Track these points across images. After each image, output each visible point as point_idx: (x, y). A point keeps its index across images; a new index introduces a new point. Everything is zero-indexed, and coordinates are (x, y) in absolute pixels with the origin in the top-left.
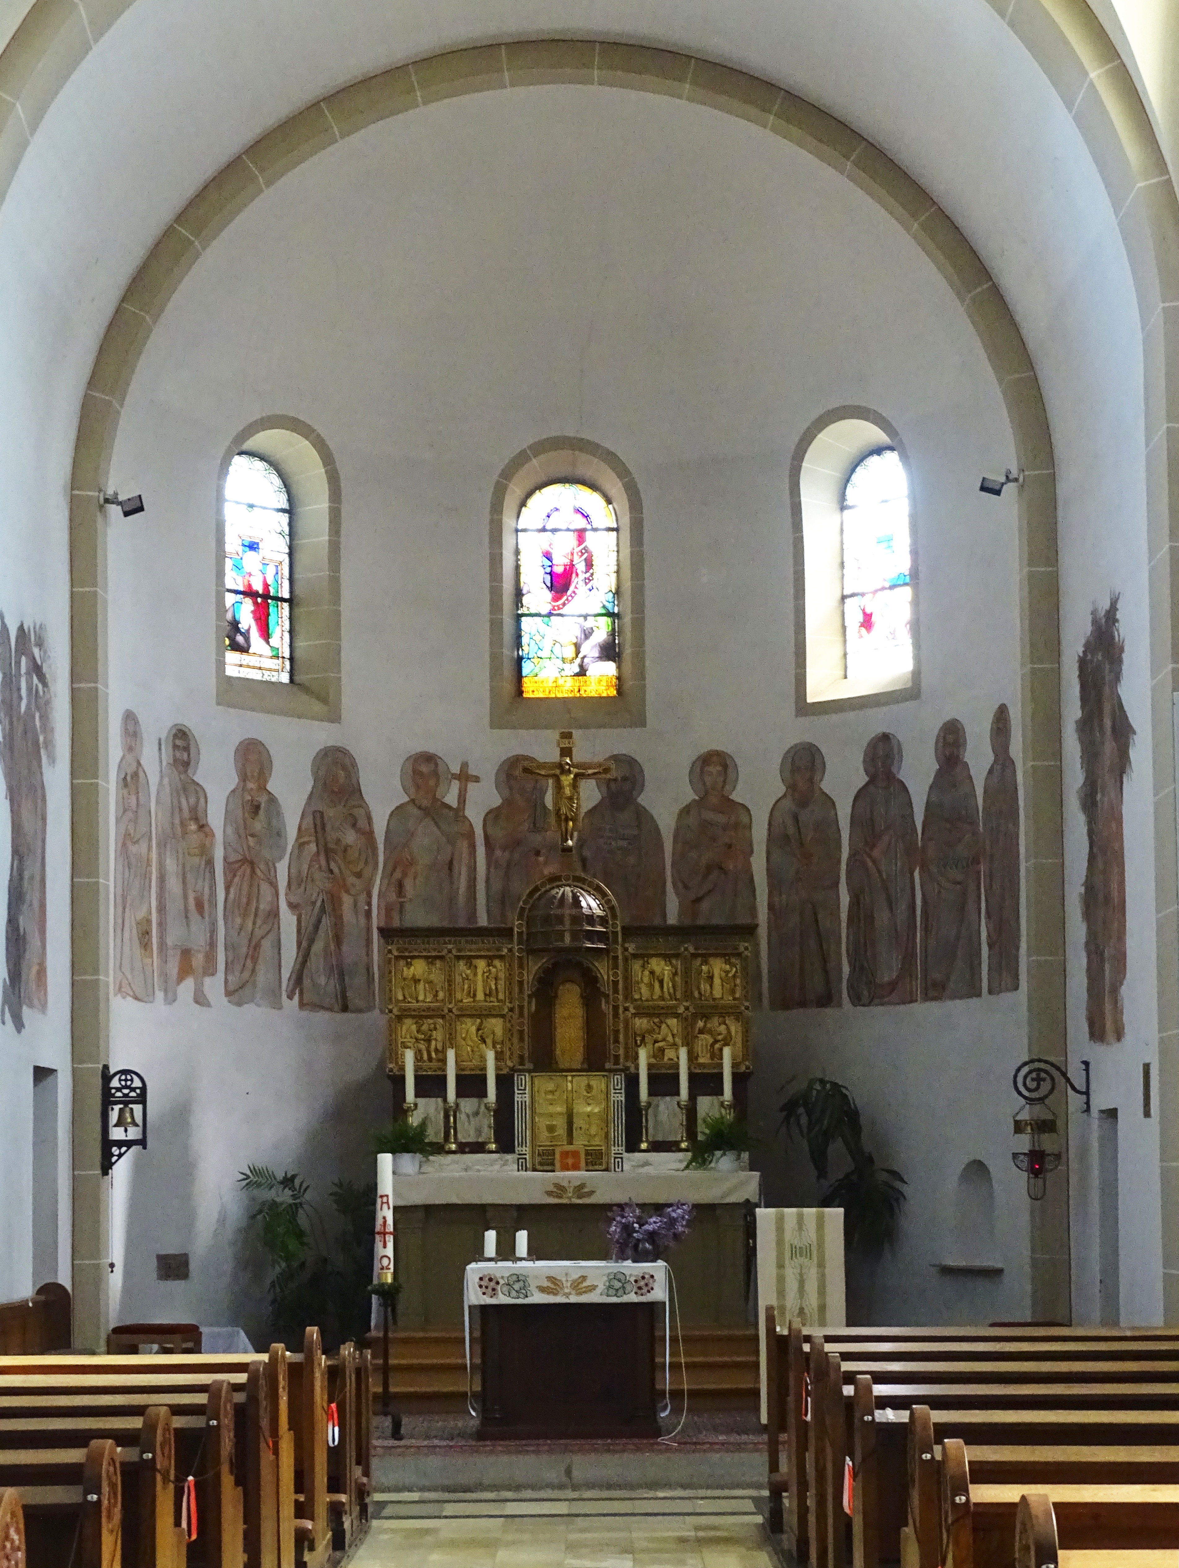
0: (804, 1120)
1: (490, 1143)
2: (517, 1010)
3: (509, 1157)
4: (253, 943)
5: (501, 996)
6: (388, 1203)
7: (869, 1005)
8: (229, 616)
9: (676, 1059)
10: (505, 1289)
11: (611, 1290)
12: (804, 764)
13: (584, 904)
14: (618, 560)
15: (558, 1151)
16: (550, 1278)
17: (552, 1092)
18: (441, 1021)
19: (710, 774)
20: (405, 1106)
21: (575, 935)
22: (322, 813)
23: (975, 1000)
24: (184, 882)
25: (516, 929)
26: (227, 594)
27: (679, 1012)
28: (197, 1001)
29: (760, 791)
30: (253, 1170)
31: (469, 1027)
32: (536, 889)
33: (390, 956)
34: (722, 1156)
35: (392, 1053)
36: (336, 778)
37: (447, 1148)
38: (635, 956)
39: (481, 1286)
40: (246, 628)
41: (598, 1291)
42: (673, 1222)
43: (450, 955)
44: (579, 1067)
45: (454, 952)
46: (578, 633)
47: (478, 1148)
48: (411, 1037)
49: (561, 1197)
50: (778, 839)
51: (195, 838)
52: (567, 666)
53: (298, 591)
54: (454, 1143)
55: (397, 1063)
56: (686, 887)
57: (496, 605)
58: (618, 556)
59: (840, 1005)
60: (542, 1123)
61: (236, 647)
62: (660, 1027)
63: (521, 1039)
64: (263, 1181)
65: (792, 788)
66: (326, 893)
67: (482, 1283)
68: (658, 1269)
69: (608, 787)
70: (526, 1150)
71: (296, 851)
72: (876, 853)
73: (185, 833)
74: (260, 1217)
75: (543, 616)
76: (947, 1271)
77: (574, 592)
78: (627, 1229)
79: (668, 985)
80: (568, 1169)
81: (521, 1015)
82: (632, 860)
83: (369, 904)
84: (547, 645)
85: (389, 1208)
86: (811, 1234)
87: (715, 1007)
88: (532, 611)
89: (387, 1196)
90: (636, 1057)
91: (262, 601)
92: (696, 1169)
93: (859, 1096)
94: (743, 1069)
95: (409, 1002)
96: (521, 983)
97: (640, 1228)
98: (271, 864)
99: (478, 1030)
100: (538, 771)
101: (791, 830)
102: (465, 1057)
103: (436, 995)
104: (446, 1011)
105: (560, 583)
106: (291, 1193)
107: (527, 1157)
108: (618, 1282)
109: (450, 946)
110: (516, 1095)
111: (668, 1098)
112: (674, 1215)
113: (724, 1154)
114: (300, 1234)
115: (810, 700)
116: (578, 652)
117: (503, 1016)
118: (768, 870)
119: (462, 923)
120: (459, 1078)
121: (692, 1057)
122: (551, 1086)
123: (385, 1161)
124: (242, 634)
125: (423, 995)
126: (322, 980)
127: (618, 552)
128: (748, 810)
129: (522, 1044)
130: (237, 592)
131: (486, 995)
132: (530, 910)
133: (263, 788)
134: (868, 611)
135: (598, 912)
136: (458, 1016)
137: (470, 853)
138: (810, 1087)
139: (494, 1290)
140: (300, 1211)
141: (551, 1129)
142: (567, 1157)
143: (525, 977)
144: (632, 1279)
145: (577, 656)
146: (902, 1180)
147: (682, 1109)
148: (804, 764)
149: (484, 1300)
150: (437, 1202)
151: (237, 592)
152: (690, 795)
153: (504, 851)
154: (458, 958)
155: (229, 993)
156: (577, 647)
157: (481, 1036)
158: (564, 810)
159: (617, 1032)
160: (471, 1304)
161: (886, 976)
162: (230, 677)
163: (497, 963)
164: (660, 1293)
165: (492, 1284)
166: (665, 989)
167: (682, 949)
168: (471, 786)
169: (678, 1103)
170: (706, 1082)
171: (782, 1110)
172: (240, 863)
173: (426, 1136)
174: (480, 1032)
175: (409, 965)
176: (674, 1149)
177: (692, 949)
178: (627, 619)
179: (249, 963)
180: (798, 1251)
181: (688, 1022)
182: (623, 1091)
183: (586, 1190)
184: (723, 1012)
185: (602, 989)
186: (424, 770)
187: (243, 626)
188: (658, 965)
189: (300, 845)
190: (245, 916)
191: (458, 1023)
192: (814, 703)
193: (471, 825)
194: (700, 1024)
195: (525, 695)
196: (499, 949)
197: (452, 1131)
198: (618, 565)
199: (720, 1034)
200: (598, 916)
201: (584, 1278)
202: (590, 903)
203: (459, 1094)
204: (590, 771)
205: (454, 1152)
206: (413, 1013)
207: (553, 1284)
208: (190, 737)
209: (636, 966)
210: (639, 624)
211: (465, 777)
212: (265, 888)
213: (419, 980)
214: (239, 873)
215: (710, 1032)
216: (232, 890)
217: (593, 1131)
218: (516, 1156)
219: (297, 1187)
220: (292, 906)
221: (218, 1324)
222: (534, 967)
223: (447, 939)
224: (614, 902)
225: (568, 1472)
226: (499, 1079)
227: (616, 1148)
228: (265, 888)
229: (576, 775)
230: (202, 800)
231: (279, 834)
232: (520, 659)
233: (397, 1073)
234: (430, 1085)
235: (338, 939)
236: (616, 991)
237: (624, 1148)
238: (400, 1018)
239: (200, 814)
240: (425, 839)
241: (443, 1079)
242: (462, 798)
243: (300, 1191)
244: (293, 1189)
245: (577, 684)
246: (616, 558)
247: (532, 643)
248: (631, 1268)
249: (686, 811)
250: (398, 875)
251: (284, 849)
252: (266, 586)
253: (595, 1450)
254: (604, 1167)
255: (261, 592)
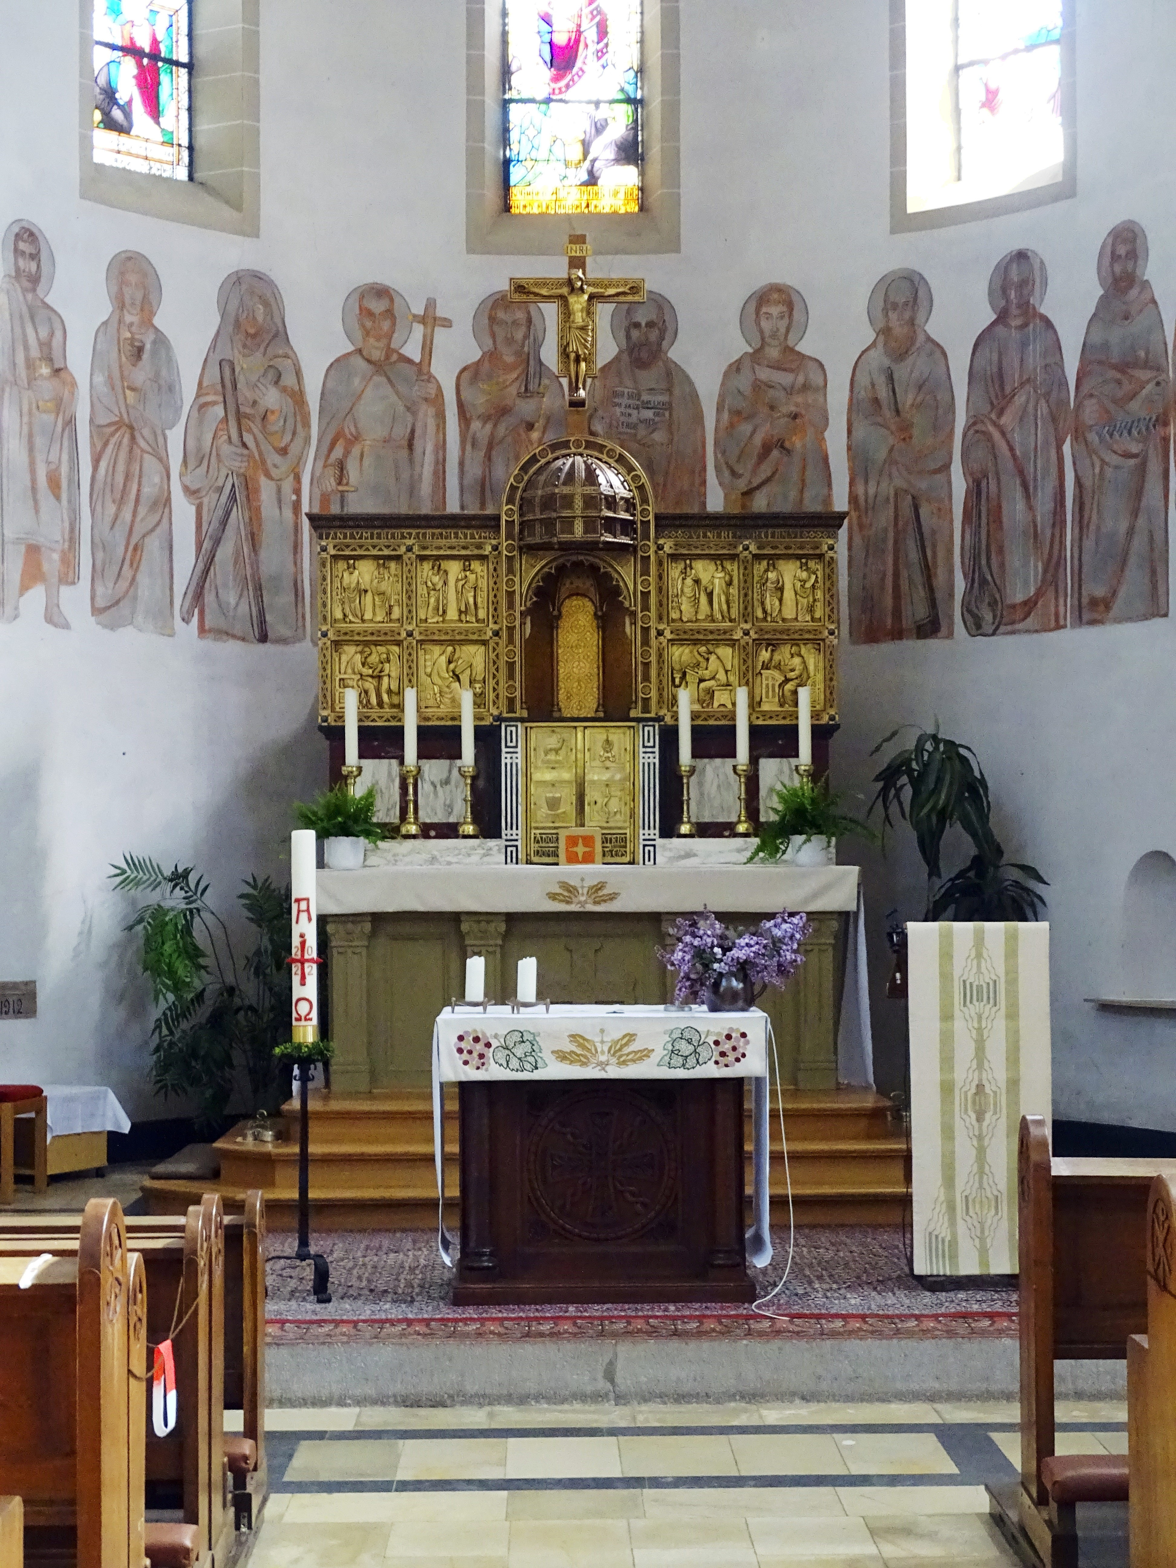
0: (908, 793)
1: (465, 823)
2: (504, 634)
3: (492, 843)
4: (133, 541)
5: (482, 614)
6: (308, 911)
7: (993, 634)
8: (102, 81)
9: (730, 706)
10: (501, 1056)
11: (675, 1057)
12: (902, 301)
13: (601, 479)
14: (642, 26)
15: (563, 834)
16: (574, 1037)
17: (557, 751)
18: (396, 649)
19: (769, 316)
20: (345, 770)
21: (590, 524)
22: (232, 365)
23: (1158, 622)
24: (31, 450)
25: (504, 518)
26: (98, 49)
27: (735, 637)
28: (49, 619)
29: (838, 341)
30: (132, 863)
31: (435, 659)
32: (534, 459)
33: (324, 555)
34: (805, 843)
35: (328, 697)
36: (253, 318)
37: (403, 831)
38: (674, 557)
39: (460, 1051)
40: (127, 99)
41: (655, 1057)
42: (776, 944)
43: (410, 554)
44: (591, 715)
45: (416, 548)
46: (587, 126)
47: (448, 831)
48: (354, 673)
49: (568, 903)
50: (865, 406)
51: (47, 387)
52: (571, 172)
53: (202, 50)
54: (415, 823)
55: (333, 710)
56: (734, 474)
57: (475, 84)
58: (642, 20)
59: (950, 635)
60: (539, 795)
61: (110, 124)
62: (708, 660)
63: (511, 676)
64: (145, 878)
65: (885, 332)
66: (238, 475)
67: (463, 1045)
68: (754, 1023)
69: (628, 337)
70: (519, 834)
71: (195, 414)
72: (1006, 420)
73: (32, 380)
74: (140, 927)
75: (540, 102)
76: (1108, 1008)
77: (581, 69)
78: (703, 957)
79: (719, 596)
80: (577, 862)
81: (511, 641)
82: (659, 436)
83: (298, 492)
84: (544, 141)
85: (310, 919)
86: (995, 965)
87: (787, 631)
88: (524, 95)
89: (308, 900)
90: (674, 701)
91: (150, 64)
92: (763, 860)
93: (985, 760)
94: (825, 719)
95: (351, 622)
96: (510, 594)
97: (724, 955)
98: (159, 432)
99: (450, 662)
100: (536, 290)
101: (883, 393)
102: (431, 703)
103: (389, 613)
104: (404, 634)
105: (562, 58)
106: (183, 894)
107: (518, 843)
108: (687, 1043)
109: (409, 542)
110: (504, 755)
111: (718, 761)
112: (778, 933)
113: (808, 840)
114: (193, 953)
115: (911, 209)
116: (586, 154)
117: (484, 643)
118: (849, 448)
119: (426, 509)
120: (422, 732)
121: (754, 704)
122: (552, 741)
123: (304, 841)
124: (120, 107)
125: (372, 613)
126: (231, 598)
127: (642, 13)
128: (821, 366)
129: (511, 683)
130: (114, 47)
131: (461, 612)
132: (524, 491)
133: (147, 322)
134: (992, 86)
135: (622, 492)
136: (421, 642)
137: (438, 426)
138: (919, 748)
139: (481, 1056)
140: (197, 920)
141: (553, 804)
142: (575, 844)
143: (517, 587)
144: (711, 1040)
145: (585, 159)
146: (1041, 880)
147: (739, 776)
148: (902, 301)
149: (465, 1073)
150: (390, 910)
151: (114, 47)
152: (739, 347)
153: (485, 423)
154: (422, 558)
155: (96, 611)
156: (586, 146)
157: (453, 672)
158: (573, 347)
159: (646, 665)
160: (444, 1080)
161: (1018, 594)
162: (102, 166)
163: (476, 565)
164: (754, 1064)
165: (479, 1047)
166: (716, 606)
167: (741, 548)
168: (440, 335)
169: (735, 767)
170: (774, 739)
171: (877, 779)
172: (113, 428)
173: (373, 814)
174: (452, 666)
175: (351, 568)
176: (727, 833)
177: (753, 548)
178: (655, 105)
179: (127, 572)
180: (974, 993)
181: (747, 655)
182: (657, 749)
183: (605, 892)
184: (796, 638)
185: (627, 604)
186: (375, 309)
187: (122, 97)
188: (704, 570)
189: (202, 407)
190: (121, 503)
191: (421, 653)
192: (915, 214)
193: (439, 388)
194: (765, 655)
195: (513, 210)
196: (479, 547)
197: (411, 806)
198: (642, 33)
199: (792, 670)
200: (622, 498)
201: (631, 1037)
202: (611, 481)
203: (422, 754)
204: (611, 291)
205: (414, 837)
206: (356, 638)
207: (580, 1046)
208: (40, 238)
209: (675, 571)
210: (672, 109)
211: (431, 319)
212: (150, 462)
213: (366, 591)
214: (113, 441)
215: (778, 667)
216: (103, 464)
217: (614, 805)
218: (501, 843)
219: (192, 886)
220: (190, 492)
221: (81, 1081)
222: (530, 571)
223: (406, 531)
224: (645, 479)
225: (610, 1376)
226: (479, 733)
227: (646, 831)
228: (150, 462)
229: (591, 297)
230: (58, 334)
231: (171, 389)
232: (507, 163)
233: (333, 724)
234: (381, 741)
235: (254, 540)
236: (646, 608)
237: (657, 831)
238: (337, 644)
239: (56, 353)
240: (375, 406)
241: (399, 732)
242: (427, 348)
243: (195, 894)
244: (186, 888)
245: (585, 197)
246: (639, 23)
247: (524, 139)
248: (703, 1019)
249: (736, 367)
250: (338, 452)
251: (178, 410)
252: (155, 43)
253: (653, 1333)
254: (627, 859)
255: (147, 50)
